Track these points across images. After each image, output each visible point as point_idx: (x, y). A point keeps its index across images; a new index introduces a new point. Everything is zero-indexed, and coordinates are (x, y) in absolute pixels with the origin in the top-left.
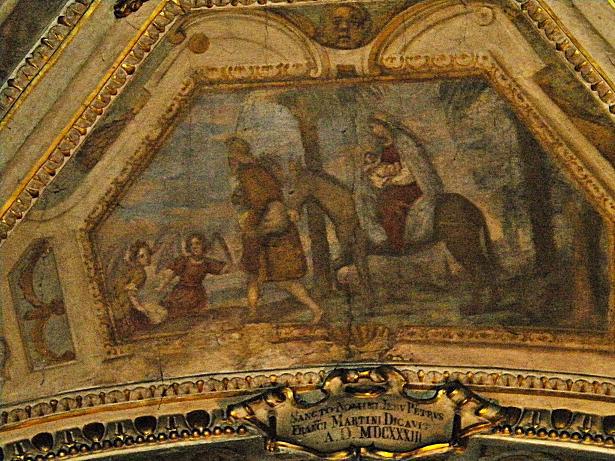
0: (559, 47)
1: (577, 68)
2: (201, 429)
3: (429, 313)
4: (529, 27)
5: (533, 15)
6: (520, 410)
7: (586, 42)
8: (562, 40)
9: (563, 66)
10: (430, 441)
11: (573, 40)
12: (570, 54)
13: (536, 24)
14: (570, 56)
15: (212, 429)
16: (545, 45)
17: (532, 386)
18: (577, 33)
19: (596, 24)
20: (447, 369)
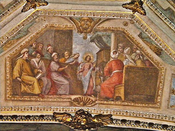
0: (9, 10)
1: (3, 15)
2: (28, 119)
3: (51, 52)
4: (14, 3)
5: (17, 4)
6: (127, 120)
7: (10, 17)
8: (10, 11)
9: (4, 11)
10: (12, 125)
11: (10, 14)
12: (7, 13)
13: (15, 5)
14: (6, 13)
15: (168, 129)
16: (9, 7)
17: (117, 114)
18: (12, 15)
19: (14, 20)
20: (147, 113)
